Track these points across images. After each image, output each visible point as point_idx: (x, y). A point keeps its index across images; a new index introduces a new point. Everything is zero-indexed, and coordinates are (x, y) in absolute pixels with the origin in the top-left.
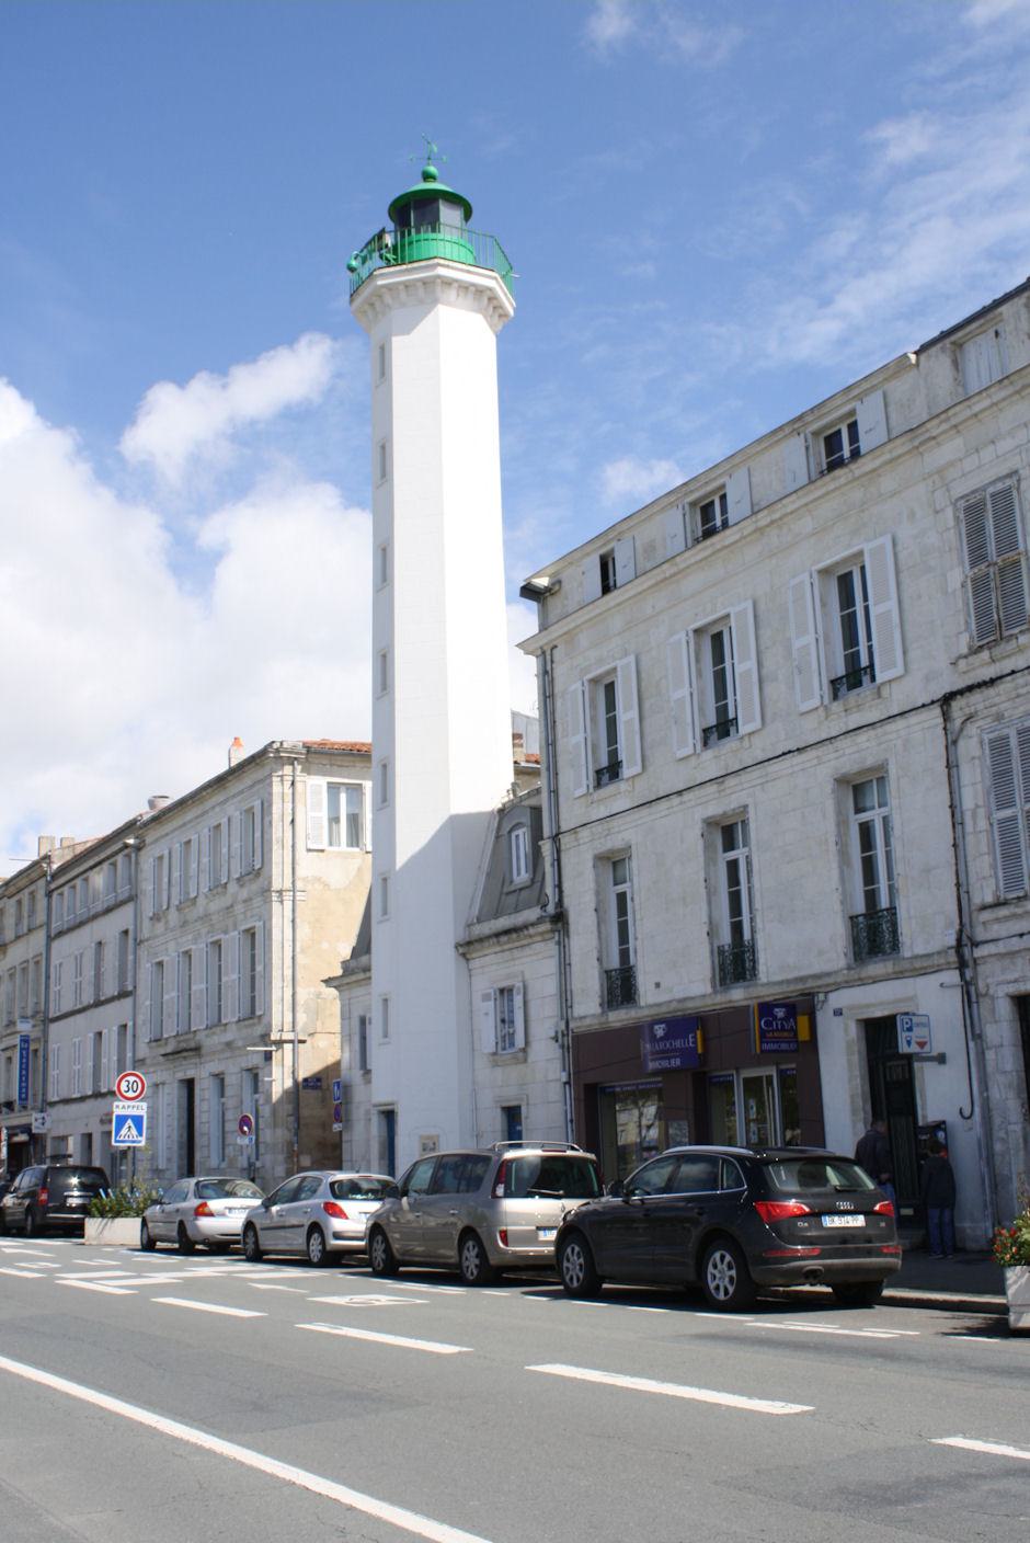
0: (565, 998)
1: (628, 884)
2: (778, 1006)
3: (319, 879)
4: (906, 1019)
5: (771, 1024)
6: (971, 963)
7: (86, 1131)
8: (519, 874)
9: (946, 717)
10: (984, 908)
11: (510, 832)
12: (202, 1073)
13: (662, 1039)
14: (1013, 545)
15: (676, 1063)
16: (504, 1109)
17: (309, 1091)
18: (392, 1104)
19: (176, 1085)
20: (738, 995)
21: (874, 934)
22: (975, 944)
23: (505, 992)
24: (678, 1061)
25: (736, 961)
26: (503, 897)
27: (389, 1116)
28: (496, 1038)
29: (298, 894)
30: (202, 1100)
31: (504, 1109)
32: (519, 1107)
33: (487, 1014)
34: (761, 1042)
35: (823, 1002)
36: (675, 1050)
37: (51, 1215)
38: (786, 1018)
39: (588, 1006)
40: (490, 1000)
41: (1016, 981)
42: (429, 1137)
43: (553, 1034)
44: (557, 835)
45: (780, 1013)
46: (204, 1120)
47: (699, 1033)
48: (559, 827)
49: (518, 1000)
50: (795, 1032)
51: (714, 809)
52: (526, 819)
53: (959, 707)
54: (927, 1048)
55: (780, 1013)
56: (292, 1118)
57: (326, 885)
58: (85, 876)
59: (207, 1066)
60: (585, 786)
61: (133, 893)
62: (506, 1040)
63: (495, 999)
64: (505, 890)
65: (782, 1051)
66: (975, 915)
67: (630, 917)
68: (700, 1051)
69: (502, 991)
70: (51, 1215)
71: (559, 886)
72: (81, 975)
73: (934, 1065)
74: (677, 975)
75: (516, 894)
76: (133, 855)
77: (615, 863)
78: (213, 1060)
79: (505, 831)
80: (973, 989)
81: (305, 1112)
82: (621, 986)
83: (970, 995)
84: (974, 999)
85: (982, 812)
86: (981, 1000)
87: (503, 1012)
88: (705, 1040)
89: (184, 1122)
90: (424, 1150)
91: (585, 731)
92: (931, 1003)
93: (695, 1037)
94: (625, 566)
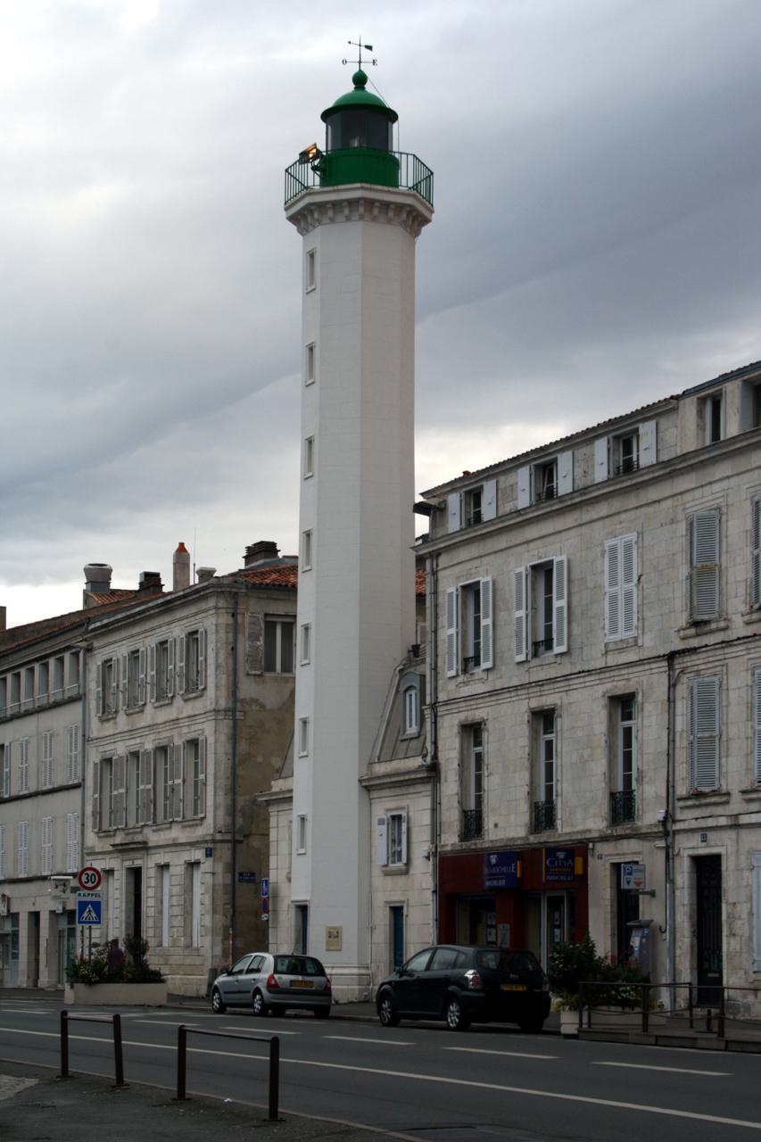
0: (436, 830)
1: (553, 735)
2: (560, 850)
3: (255, 701)
4: (628, 866)
5: (554, 863)
6: (671, 833)
7: (33, 909)
8: (411, 726)
9: (671, 667)
10: (679, 800)
11: (405, 691)
12: (149, 864)
13: (495, 865)
14: (711, 558)
15: (502, 883)
16: (391, 908)
17: (245, 884)
18: (306, 901)
19: (124, 872)
20: (545, 837)
21: (622, 806)
22: (674, 821)
23: (397, 819)
24: (504, 882)
25: (543, 815)
26: (398, 742)
27: (303, 909)
28: (388, 853)
29: (238, 713)
30: (148, 887)
31: (391, 908)
32: (402, 908)
33: (381, 835)
34: (546, 875)
35: (593, 849)
36: (503, 874)
37: (401, 1012)
38: (566, 859)
39: (451, 839)
40: (384, 824)
41: (693, 848)
42: (333, 928)
43: (426, 855)
44: (435, 703)
45: (561, 855)
46: (150, 904)
47: (518, 863)
48: (437, 698)
49: (404, 826)
50: (573, 868)
51: (534, 703)
52: (416, 684)
53: (679, 664)
54: (642, 886)
55: (561, 855)
56: (229, 906)
57: (263, 706)
58: (16, 671)
59: (153, 857)
60: (524, 655)
61: (81, 692)
62: (396, 856)
63: (388, 825)
64: (400, 738)
65: (561, 881)
66: (676, 802)
67: (634, 749)
68: (518, 875)
69: (393, 817)
70: (401, 1012)
71: (435, 743)
72: (26, 760)
73: (647, 897)
74: (507, 823)
75: (407, 742)
76: (81, 655)
77: (473, 731)
78: (160, 853)
79: (402, 689)
80: (671, 850)
81: (239, 902)
82: (472, 823)
83: (669, 856)
84: (671, 857)
85: (685, 734)
86: (675, 858)
87: (393, 834)
88: (522, 868)
89: (132, 905)
90: (330, 937)
91: (527, 609)
92: (650, 856)
93: (516, 866)
94: (565, 477)
